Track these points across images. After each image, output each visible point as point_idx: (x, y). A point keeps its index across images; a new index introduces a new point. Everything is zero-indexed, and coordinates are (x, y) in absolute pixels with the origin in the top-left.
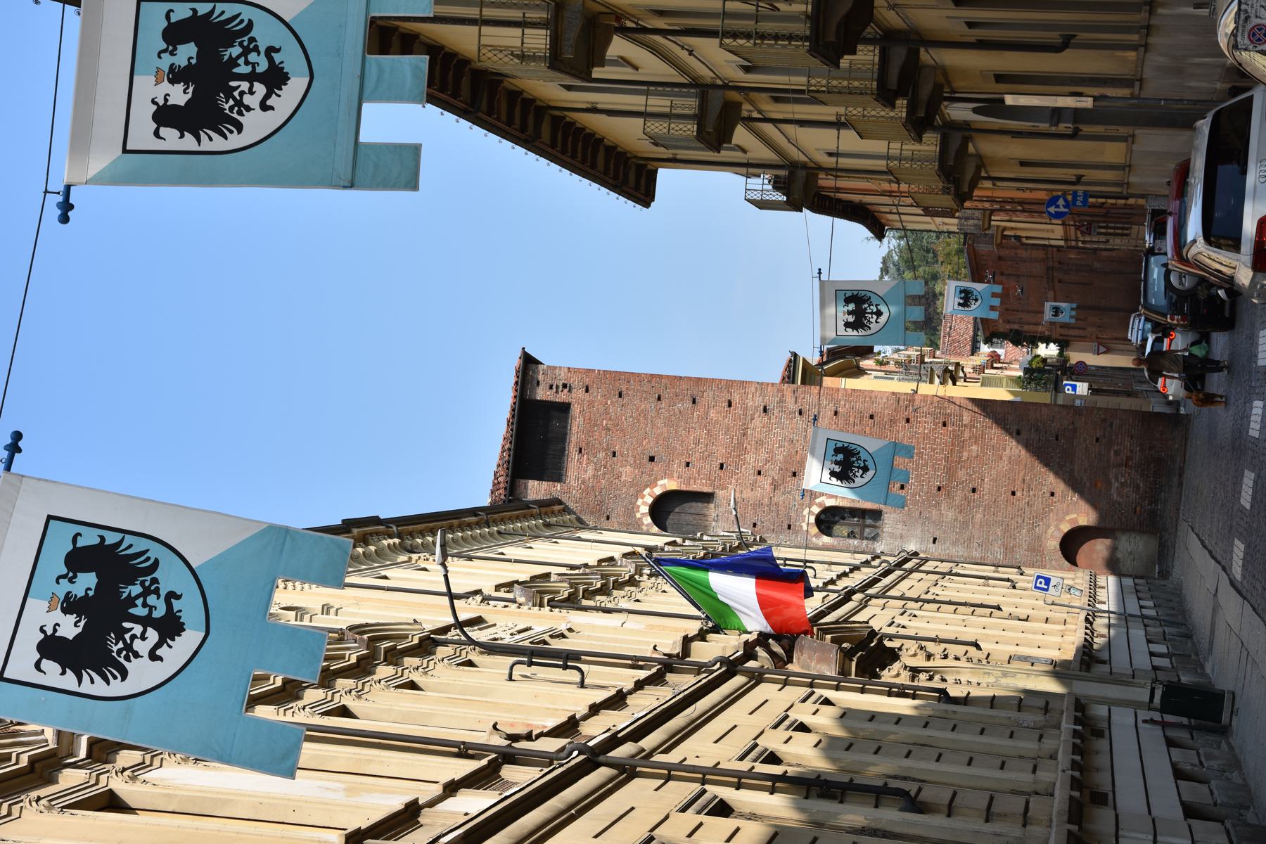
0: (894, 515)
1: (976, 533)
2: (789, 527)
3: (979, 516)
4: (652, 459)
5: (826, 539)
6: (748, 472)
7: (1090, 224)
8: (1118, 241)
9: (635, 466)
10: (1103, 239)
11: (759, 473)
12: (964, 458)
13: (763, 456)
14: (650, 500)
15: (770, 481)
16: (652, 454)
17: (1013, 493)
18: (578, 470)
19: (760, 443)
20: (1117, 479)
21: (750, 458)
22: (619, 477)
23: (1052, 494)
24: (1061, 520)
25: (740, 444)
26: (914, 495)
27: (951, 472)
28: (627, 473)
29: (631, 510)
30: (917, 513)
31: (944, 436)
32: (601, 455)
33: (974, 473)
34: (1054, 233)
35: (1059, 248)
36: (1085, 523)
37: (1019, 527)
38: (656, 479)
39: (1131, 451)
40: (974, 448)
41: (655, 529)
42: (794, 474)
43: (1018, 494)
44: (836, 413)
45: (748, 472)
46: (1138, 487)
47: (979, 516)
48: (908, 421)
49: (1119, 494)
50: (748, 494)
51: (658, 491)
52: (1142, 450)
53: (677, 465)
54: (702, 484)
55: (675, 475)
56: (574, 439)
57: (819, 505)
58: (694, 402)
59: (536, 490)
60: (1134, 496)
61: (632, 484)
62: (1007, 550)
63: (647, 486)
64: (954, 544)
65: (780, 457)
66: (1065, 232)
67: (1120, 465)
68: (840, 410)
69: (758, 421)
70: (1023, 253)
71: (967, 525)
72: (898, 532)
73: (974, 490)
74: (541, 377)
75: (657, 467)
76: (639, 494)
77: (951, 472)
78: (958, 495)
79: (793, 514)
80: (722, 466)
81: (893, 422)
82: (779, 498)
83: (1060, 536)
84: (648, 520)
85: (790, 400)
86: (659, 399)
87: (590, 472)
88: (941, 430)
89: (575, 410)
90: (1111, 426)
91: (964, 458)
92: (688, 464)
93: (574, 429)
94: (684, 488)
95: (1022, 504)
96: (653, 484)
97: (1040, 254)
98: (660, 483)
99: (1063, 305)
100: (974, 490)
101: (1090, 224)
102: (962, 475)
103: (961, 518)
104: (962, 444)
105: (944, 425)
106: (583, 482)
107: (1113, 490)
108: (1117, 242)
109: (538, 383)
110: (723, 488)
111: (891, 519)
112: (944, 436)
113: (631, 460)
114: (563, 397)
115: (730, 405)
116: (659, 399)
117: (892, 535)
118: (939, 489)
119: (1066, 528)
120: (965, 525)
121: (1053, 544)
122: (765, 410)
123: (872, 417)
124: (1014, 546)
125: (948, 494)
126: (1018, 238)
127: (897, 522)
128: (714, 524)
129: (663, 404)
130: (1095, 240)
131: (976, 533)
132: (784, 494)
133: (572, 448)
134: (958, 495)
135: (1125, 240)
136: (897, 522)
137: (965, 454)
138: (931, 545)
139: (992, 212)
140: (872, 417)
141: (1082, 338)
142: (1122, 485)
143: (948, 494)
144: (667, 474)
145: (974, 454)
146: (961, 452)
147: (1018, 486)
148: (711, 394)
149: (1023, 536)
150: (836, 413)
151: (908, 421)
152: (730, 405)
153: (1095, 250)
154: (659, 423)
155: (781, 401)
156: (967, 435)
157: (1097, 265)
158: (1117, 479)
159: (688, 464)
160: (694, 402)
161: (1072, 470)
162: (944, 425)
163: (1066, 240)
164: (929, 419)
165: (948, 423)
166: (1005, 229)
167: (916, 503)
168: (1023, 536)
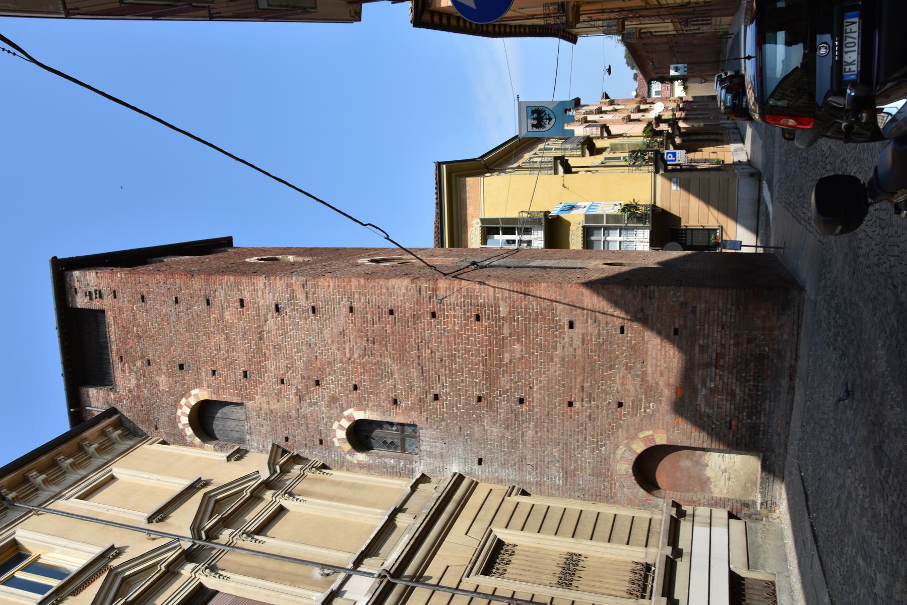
0: (430, 431)
1: (528, 454)
2: (321, 442)
3: (530, 433)
4: (181, 367)
5: (361, 457)
6: (270, 379)
7: (687, 20)
8: (705, 27)
9: (170, 375)
10: (696, 27)
11: (282, 382)
12: (506, 361)
13: (284, 362)
14: (188, 411)
15: (294, 391)
16: (181, 361)
17: (570, 404)
18: (125, 378)
19: (278, 347)
20: (704, 384)
21: (271, 365)
22: (157, 386)
23: (620, 405)
24: (634, 438)
25: (259, 349)
26: (450, 407)
27: (491, 379)
28: (163, 381)
29: (174, 421)
30: (457, 429)
31: (478, 333)
32: (139, 363)
33: (520, 379)
34: (667, 27)
35: (674, 35)
36: (664, 442)
37: (581, 447)
38: (189, 389)
39: (723, 346)
40: (517, 347)
41: (197, 441)
42: (317, 383)
43: (577, 405)
44: (351, 309)
45: (270, 379)
46: (733, 394)
47: (530, 433)
48: (434, 315)
49: (708, 404)
50: (275, 405)
51: (193, 401)
52: (737, 344)
53: (205, 375)
54: (230, 394)
55: (205, 384)
56: (114, 347)
57: (348, 418)
58: (208, 303)
59: (97, 399)
60: (728, 407)
61: (171, 394)
62: (567, 474)
63: (182, 396)
64: (503, 465)
65: (300, 364)
66: (675, 26)
67: (708, 365)
68: (355, 305)
69: (272, 323)
70: (654, 40)
71: (517, 443)
72: (437, 451)
73: (521, 401)
74: (77, 285)
75: (188, 378)
76: (176, 405)
77: (491, 379)
78: (503, 408)
79: (324, 431)
80: (245, 374)
81: (416, 317)
82: (306, 410)
83: (633, 458)
84: (189, 431)
85: (301, 296)
86: (176, 301)
87: (133, 382)
88: (475, 326)
89: (110, 317)
90: (694, 311)
91: (506, 361)
92: (214, 373)
93: (113, 337)
94: (214, 398)
95: (583, 418)
96: (186, 393)
97: (665, 40)
98: (193, 392)
99: (680, 65)
100: (521, 401)
101: (687, 20)
102: (504, 381)
103: (508, 435)
104: (502, 344)
105: (478, 318)
106: (130, 391)
107: (700, 400)
108: (705, 29)
109: (76, 293)
110: (252, 399)
111: (427, 437)
112: (478, 333)
113: (164, 368)
114: (96, 305)
115: (242, 306)
116: (176, 301)
117: (430, 455)
118: (480, 399)
119: (639, 448)
120: (514, 444)
121: (624, 467)
122: (277, 309)
123: (391, 312)
124: (576, 469)
125: (491, 406)
126: (651, 33)
127: (435, 439)
128: (248, 437)
129: (182, 307)
130: (692, 29)
131: (528, 454)
132: (310, 405)
133: (114, 357)
134: (503, 408)
135: (709, 27)
136: (435, 439)
137: (507, 356)
138: (476, 467)
139: (624, 20)
140: (391, 312)
141: (693, 77)
142: (712, 391)
143: (491, 406)
144: (198, 384)
145: (518, 356)
146: (500, 353)
147: (575, 396)
148: (222, 292)
149: (586, 457)
150: (351, 309)
151: (434, 315)
152: (242, 306)
153: (694, 34)
154: (181, 327)
155: (292, 297)
156: (506, 331)
157: (696, 42)
158: (704, 384)
159: (214, 373)
160: (208, 303)
161: (644, 373)
162: (478, 318)
163: (676, 31)
164: (459, 313)
165: (482, 315)
166: (641, 29)
167: (454, 417)
168: (586, 457)
